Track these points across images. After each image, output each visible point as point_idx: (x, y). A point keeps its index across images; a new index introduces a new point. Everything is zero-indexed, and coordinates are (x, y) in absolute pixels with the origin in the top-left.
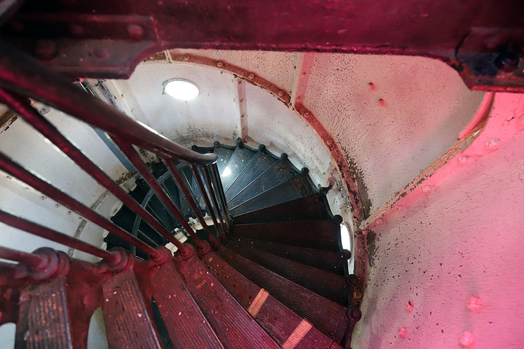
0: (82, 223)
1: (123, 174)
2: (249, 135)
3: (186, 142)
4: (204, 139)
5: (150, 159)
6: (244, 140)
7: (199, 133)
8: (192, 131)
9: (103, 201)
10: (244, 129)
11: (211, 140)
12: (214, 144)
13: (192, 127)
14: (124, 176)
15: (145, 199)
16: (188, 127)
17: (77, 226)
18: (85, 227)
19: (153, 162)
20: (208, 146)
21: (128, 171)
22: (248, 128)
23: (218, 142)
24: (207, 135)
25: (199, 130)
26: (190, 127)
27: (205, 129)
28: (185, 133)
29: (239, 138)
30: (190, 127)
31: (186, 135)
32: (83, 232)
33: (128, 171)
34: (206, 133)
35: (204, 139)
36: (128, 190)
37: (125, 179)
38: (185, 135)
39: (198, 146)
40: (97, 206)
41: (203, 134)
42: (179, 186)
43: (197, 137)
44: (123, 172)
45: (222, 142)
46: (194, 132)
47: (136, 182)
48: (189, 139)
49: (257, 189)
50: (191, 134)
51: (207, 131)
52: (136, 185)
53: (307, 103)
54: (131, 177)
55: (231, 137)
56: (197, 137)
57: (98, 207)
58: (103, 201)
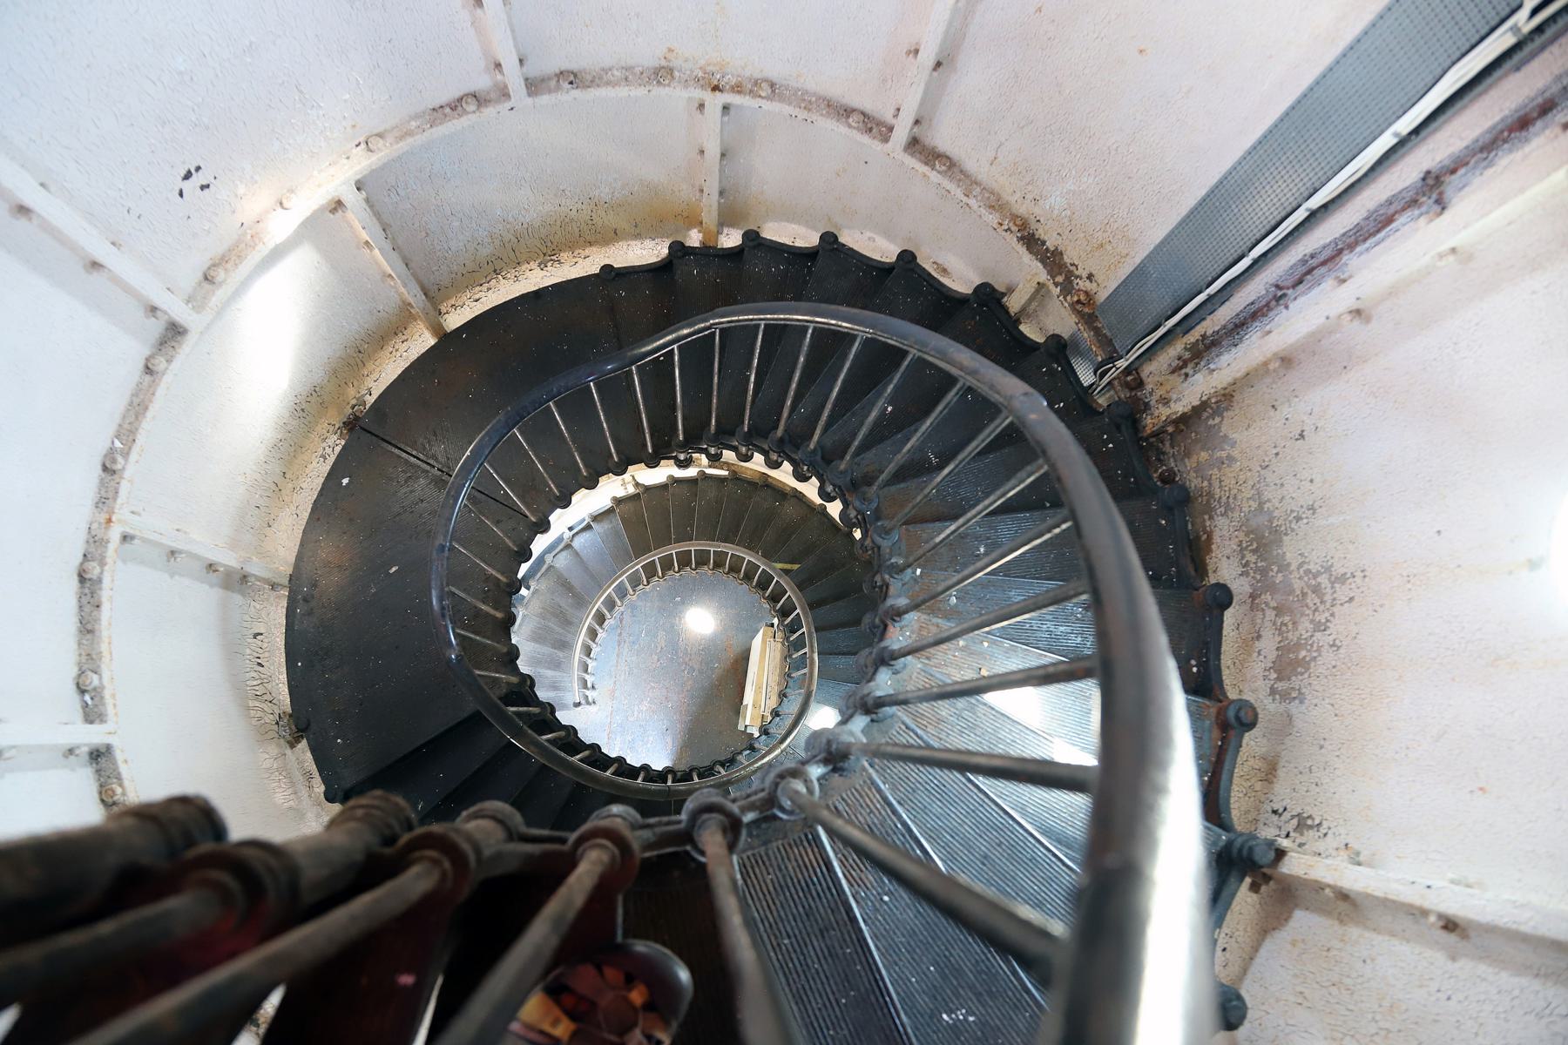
0: (879, 123)
1: (1090, 277)
2: (1302, 920)
3: (1251, 558)
4: (1268, 645)
5: (1160, 392)
6: (1267, 878)
7: (1305, 626)
8: (1316, 590)
9: (972, 202)
10: (1345, 905)
11: (1263, 687)
12: (1244, 705)
13: (1342, 593)
14: (1083, 284)
15: (1020, 475)
16: (1338, 570)
17: (868, 106)
18: (865, 139)
19: (1147, 405)
20: (1226, 660)
21: (1102, 296)
22: (1354, 932)
23: (1251, 725)
24: (1289, 665)
25: (1321, 627)
26: (1342, 579)
27: (1328, 657)
28: (1304, 549)
29: (1280, 854)
30: (1342, 579)
31: (1291, 556)
32: (843, 129)
33: (1102, 296)
34: (1305, 664)
35: (1268, 645)
36: (1023, 310)
37: (1067, 288)
38: (1290, 550)
39: (1229, 616)
40: (951, 178)
41: (1298, 646)
42: (970, 448)
43: (1279, 611)
44: (1099, 277)
45: (1253, 744)
46: (1312, 599)
47: (1055, 339)
48: (1264, 572)
49: (958, 972)
50: (1298, 585)
51: (1319, 668)
52: (1040, 339)
53: (943, 137)
54: (1079, 313)
55: (1282, 793)
56: (1279, 611)
57: (947, 184)
58: (972, 202)
